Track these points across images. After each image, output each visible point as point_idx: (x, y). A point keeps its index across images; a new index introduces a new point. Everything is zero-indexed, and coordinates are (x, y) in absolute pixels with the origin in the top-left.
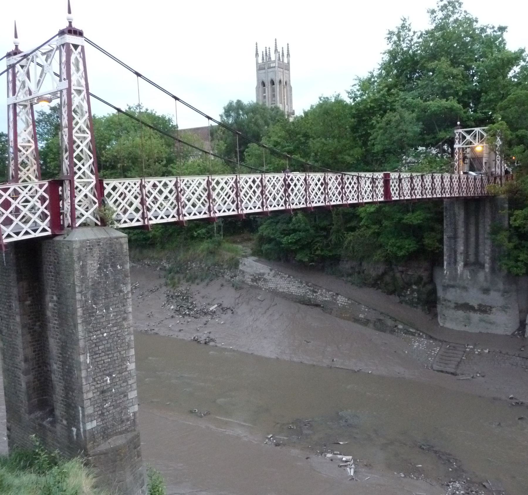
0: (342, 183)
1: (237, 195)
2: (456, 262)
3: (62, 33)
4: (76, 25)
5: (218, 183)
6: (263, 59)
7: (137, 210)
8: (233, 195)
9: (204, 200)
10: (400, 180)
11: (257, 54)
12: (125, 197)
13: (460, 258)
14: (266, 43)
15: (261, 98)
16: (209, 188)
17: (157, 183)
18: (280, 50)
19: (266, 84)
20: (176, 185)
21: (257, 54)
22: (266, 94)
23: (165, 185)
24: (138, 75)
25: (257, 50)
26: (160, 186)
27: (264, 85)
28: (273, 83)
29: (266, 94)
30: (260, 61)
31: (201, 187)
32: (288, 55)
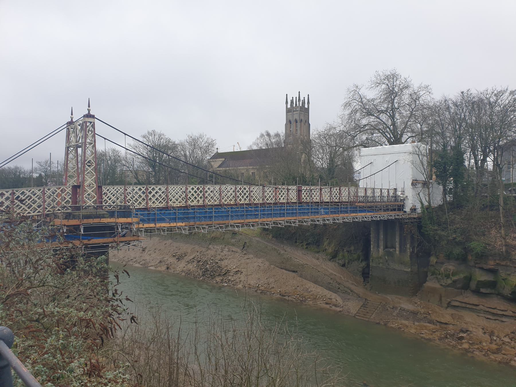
2: (378, 247)
3: (84, 116)
4: (91, 113)
7: (144, 199)
9: (21, 207)
11: (287, 102)
12: (107, 195)
13: (381, 243)
14: (293, 95)
17: (142, 188)
19: (292, 122)
21: (287, 102)
24: (125, 134)
25: (287, 99)
30: (289, 106)
31: (232, 196)
32: (308, 102)
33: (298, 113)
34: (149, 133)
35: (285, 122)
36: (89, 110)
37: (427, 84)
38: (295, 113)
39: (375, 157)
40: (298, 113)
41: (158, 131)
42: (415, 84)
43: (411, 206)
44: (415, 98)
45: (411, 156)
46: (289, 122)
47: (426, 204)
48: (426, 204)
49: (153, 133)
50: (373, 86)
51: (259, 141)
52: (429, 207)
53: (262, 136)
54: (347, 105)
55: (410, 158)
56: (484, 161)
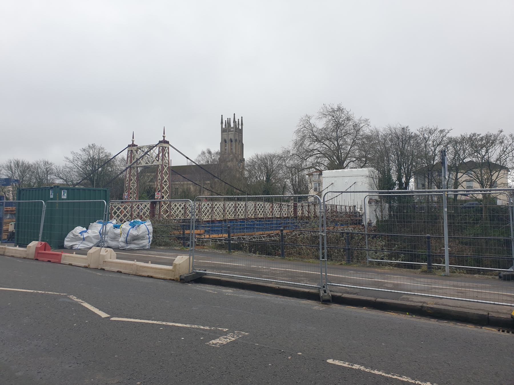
0: (272, 207)
1: (224, 211)
5: (239, 204)
6: (226, 125)
8: (222, 211)
10: (302, 206)
11: (222, 123)
15: (223, 150)
16: (235, 207)
18: (237, 120)
19: (227, 141)
20: (184, 206)
22: (227, 148)
23: (242, 205)
26: (178, 206)
27: (226, 142)
28: (231, 141)
29: (227, 148)
30: (224, 127)
31: (146, 208)
32: (242, 124)
33: (232, 134)
34: (89, 146)
35: (220, 140)
36: (164, 137)
37: (367, 118)
38: (230, 133)
39: (336, 179)
40: (232, 134)
41: (98, 145)
42: (356, 118)
43: (368, 221)
44: (357, 128)
45: (368, 179)
46: (224, 142)
47: (380, 218)
48: (380, 218)
49: (93, 147)
50: (320, 116)
51: (200, 158)
52: (382, 221)
53: (203, 153)
54: (298, 131)
55: (367, 180)
56: (407, 183)
